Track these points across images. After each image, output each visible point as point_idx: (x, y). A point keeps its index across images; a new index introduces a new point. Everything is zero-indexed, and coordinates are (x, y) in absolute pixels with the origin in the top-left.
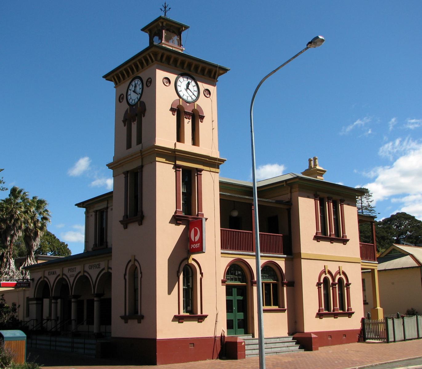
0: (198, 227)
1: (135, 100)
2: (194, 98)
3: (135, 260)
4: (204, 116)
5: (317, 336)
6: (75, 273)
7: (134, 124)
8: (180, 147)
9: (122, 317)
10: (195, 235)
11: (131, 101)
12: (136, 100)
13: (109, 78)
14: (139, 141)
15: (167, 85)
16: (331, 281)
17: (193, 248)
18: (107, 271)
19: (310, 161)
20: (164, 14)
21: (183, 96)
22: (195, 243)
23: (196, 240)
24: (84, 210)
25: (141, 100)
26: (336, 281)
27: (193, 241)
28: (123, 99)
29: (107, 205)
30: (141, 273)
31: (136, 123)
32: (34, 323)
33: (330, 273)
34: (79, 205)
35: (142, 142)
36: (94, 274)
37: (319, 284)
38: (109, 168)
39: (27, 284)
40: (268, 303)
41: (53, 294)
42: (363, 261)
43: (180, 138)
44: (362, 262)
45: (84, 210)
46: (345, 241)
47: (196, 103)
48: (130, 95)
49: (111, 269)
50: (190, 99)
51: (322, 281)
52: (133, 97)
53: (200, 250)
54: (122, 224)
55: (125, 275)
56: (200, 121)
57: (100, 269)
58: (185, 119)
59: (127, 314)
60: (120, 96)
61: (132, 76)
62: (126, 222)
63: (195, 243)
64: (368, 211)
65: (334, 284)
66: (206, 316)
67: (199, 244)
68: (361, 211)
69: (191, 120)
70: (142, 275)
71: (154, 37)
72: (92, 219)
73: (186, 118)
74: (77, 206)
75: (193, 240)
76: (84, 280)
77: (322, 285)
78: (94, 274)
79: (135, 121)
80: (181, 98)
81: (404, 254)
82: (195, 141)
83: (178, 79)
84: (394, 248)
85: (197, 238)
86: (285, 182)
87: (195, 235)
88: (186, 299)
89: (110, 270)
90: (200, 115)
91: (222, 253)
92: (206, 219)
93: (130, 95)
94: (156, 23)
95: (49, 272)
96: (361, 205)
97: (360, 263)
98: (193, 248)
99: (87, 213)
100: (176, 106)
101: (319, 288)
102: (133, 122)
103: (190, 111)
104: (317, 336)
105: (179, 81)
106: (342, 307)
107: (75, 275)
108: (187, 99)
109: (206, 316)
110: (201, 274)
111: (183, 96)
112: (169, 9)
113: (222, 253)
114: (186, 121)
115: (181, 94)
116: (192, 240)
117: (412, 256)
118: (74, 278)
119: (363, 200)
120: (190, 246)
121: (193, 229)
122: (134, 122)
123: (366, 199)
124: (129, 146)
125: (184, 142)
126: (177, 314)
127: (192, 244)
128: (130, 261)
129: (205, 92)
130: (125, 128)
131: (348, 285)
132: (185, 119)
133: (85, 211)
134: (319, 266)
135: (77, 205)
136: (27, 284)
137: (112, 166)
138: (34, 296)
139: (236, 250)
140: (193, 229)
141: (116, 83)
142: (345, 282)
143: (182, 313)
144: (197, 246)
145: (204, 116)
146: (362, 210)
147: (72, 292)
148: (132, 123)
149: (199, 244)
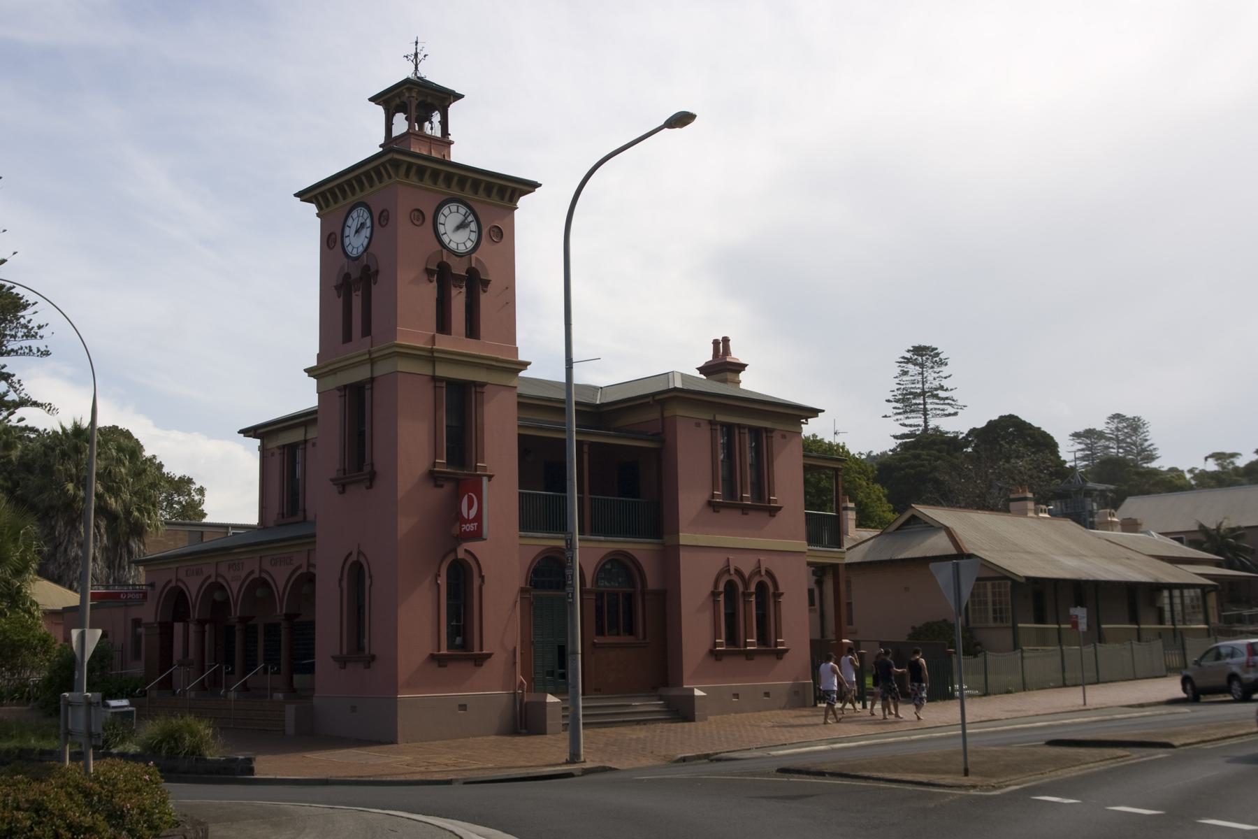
0: (476, 496)
1: (358, 248)
2: (470, 245)
3: (359, 553)
4: (490, 281)
5: (705, 694)
6: (243, 574)
7: (357, 295)
8: (444, 343)
9: (335, 658)
10: (470, 506)
11: (349, 249)
12: (361, 249)
13: (307, 196)
14: (367, 331)
15: (418, 223)
16: (741, 589)
17: (465, 530)
18: (305, 571)
19: (716, 343)
20: (414, 66)
21: (449, 244)
22: (469, 521)
23: (471, 517)
24: (257, 442)
25: (370, 250)
26: (753, 588)
27: (463, 517)
28: (335, 242)
29: (305, 437)
30: (371, 577)
31: (359, 293)
32: (745, 608)
33: (738, 572)
34: (248, 432)
35: (372, 334)
36: (281, 577)
37: (714, 594)
38: (309, 376)
39: (141, 595)
40: (600, 631)
41: (195, 614)
42: (810, 548)
43: (443, 325)
44: (809, 550)
45: (257, 442)
46: (773, 511)
47: (474, 255)
48: (349, 236)
49: (314, 566)
50: (462, 249)
51: (721, 588)
52: (356, 243)
53: (477, 535)
54: (334, 484)
55: (341, 580)
56: (483, 290)
57: (293, 567)
58: (452, 286)
59: (345, 652)
60: (330, 235)
61: (351, 199)
62: (342, 485)
63: (469, 521)
64: (937, 401)
65: (746, 595)
66: (489, 656)
67: (476, 524)
68: (922, 402)
69: (464, 290)
70: (371, 581)
71: (393, 115)
72: (276, 461)
73: (455, 287)
74: (242, 435)
75: (466, 517)
76: (258, 586)
77: (722, 597)
78: (281, 577)
79: (359, 290)
80: (445, 248)
81: (933, 527)
82: (473, 330)
83: (440, 210)
84: (914, 513)
85: (473, 513)
86: (651, 398)
87: (470, 506)
88: (839, 538)
89: (312, 570)
90: (481, 279)
91: (521, 537)
92: (490, 477)
93: (349, 236)
94: (400, 90)
95: (187, 571)
96: (921, 386)
97: (805, 552)
98: (465, 530)
99: (263, 451)
100: (436, 264)
101: (716, 603)
102: (355, 292)
103: (463, 272)
104: (705, 694)
105: (442, 213)
106: (763, 638)
107: (243, 577)
108: (458, 249)
109: (489, 656)
110: (482, 577)
111: (449, 244)
112: (425, 56)
113: (521, 537)
114: (454, 292)
115: (446, 239)
116: (464, 514)
117: (948, 531)
118: (240, 582)
119: (925, 374)
120: (461, 527)
121: (466, 496)
122: (357, 293)
123: (935, 372)
124: (347, 337)
125: (450, 334)
126: (338, 653)
127: (463, 524)
128: (350, 554)
129: (494, 231)
130: (340, 301)
131: (778, 595)
132: (452, 286)
133: (259, 444)
134: (715, 564)
135: (241, 432)
136: (141, 595)
137: (316, 373)
138: (341, 650)
139: (551, 531)
140: (466, 496)
141: (319, 207)
142: (771, 589)
143: (444, 651)
144: (471, 527)
145: (490, 281)
146: (924, 400)
147: (236, 612)
148: (354, 294)
149: (476, 524)
